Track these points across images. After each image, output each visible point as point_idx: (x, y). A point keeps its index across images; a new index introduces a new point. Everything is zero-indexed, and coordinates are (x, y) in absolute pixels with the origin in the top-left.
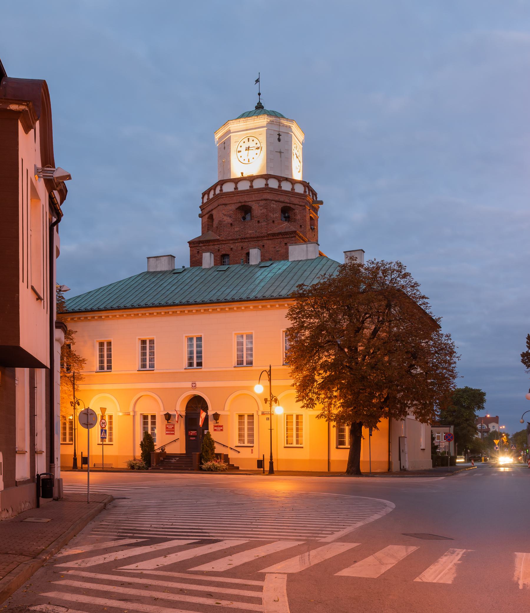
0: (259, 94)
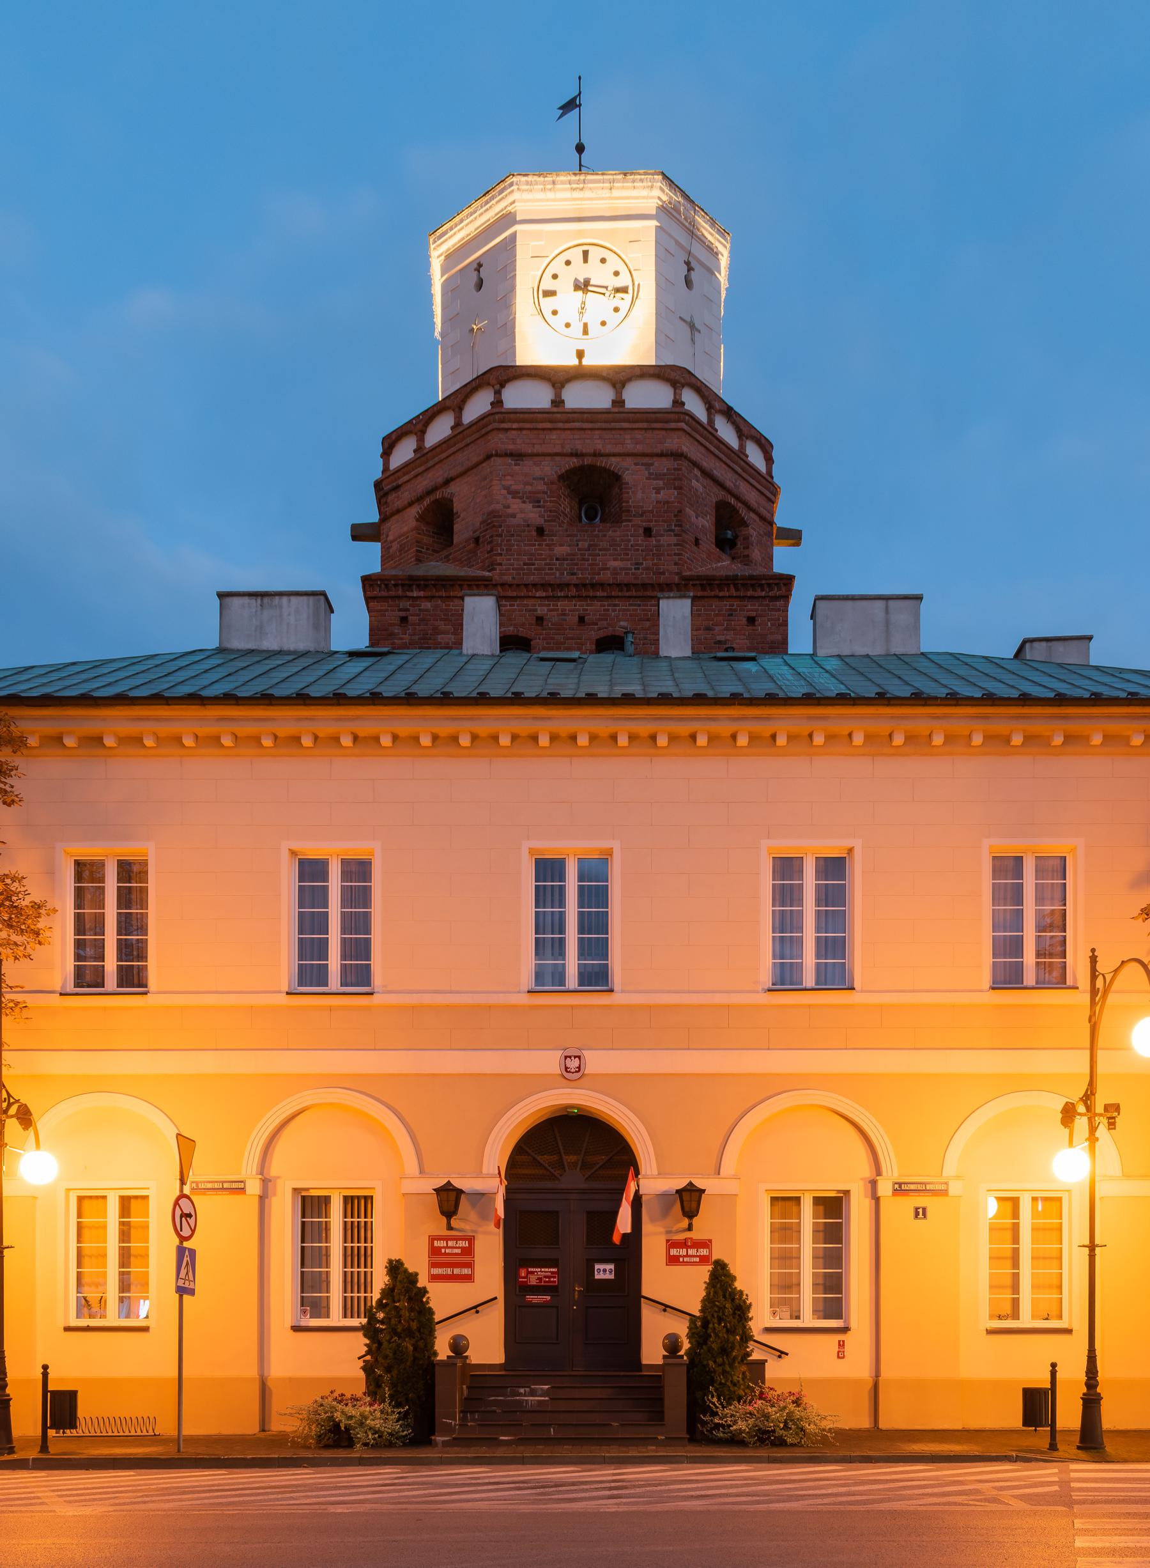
0: (580, 149)
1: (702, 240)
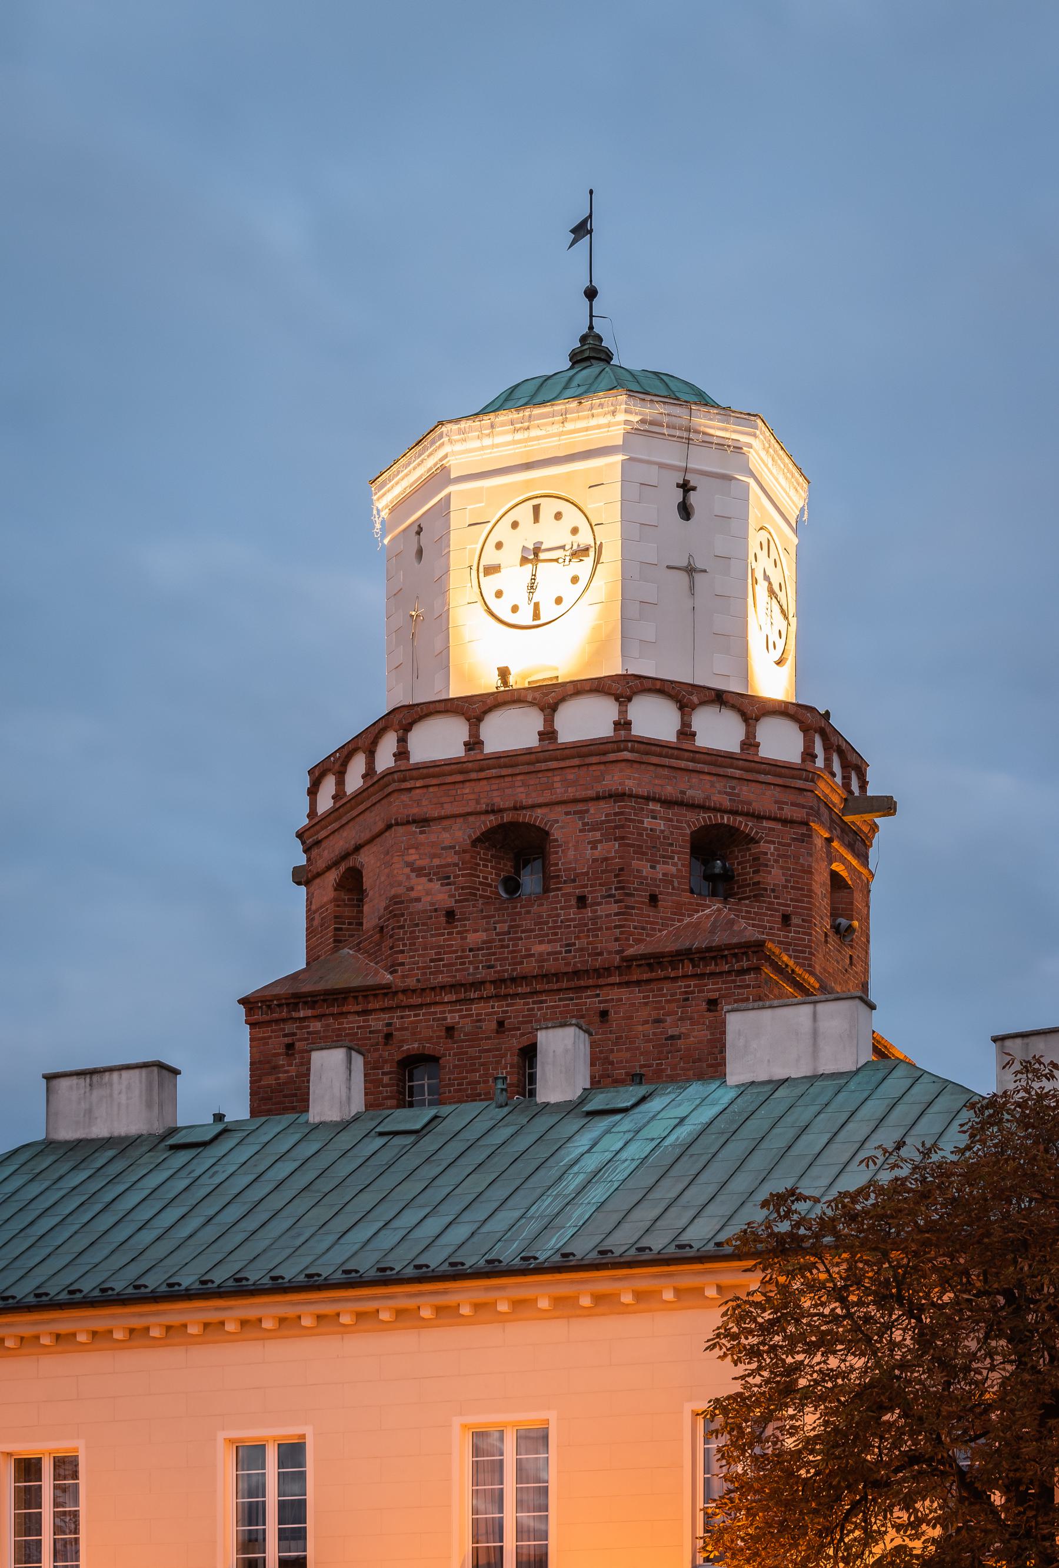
0: (591, 294)
1: (707, 442)
